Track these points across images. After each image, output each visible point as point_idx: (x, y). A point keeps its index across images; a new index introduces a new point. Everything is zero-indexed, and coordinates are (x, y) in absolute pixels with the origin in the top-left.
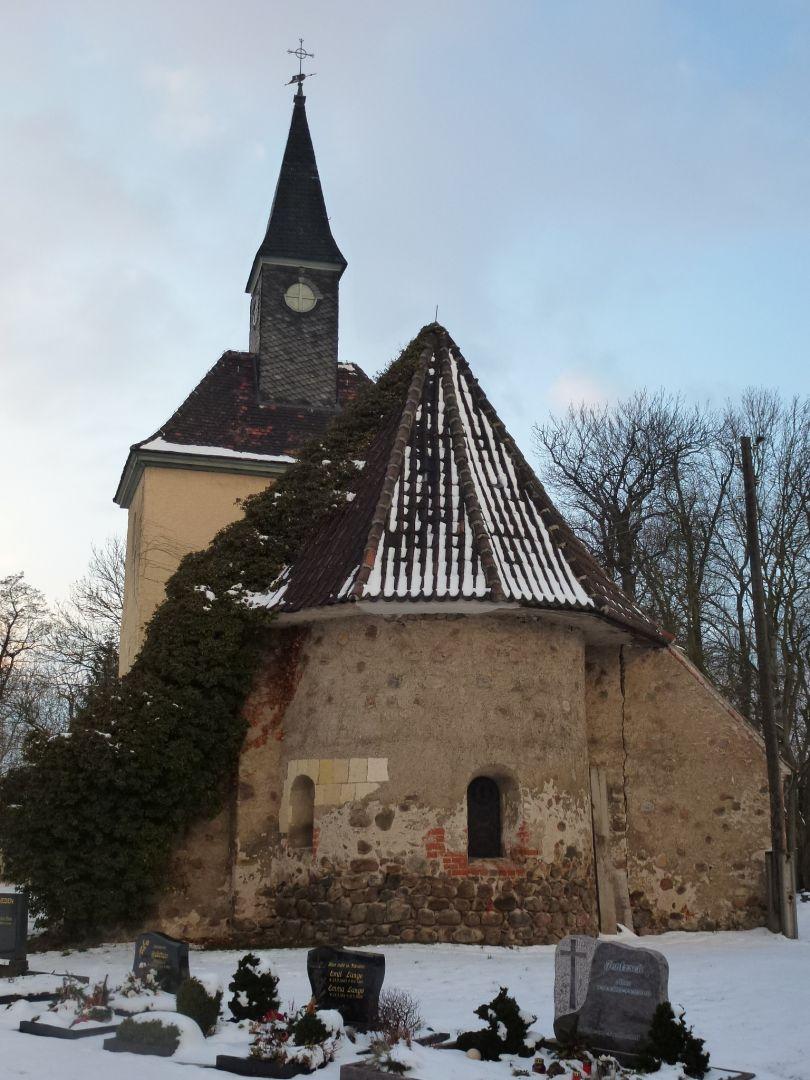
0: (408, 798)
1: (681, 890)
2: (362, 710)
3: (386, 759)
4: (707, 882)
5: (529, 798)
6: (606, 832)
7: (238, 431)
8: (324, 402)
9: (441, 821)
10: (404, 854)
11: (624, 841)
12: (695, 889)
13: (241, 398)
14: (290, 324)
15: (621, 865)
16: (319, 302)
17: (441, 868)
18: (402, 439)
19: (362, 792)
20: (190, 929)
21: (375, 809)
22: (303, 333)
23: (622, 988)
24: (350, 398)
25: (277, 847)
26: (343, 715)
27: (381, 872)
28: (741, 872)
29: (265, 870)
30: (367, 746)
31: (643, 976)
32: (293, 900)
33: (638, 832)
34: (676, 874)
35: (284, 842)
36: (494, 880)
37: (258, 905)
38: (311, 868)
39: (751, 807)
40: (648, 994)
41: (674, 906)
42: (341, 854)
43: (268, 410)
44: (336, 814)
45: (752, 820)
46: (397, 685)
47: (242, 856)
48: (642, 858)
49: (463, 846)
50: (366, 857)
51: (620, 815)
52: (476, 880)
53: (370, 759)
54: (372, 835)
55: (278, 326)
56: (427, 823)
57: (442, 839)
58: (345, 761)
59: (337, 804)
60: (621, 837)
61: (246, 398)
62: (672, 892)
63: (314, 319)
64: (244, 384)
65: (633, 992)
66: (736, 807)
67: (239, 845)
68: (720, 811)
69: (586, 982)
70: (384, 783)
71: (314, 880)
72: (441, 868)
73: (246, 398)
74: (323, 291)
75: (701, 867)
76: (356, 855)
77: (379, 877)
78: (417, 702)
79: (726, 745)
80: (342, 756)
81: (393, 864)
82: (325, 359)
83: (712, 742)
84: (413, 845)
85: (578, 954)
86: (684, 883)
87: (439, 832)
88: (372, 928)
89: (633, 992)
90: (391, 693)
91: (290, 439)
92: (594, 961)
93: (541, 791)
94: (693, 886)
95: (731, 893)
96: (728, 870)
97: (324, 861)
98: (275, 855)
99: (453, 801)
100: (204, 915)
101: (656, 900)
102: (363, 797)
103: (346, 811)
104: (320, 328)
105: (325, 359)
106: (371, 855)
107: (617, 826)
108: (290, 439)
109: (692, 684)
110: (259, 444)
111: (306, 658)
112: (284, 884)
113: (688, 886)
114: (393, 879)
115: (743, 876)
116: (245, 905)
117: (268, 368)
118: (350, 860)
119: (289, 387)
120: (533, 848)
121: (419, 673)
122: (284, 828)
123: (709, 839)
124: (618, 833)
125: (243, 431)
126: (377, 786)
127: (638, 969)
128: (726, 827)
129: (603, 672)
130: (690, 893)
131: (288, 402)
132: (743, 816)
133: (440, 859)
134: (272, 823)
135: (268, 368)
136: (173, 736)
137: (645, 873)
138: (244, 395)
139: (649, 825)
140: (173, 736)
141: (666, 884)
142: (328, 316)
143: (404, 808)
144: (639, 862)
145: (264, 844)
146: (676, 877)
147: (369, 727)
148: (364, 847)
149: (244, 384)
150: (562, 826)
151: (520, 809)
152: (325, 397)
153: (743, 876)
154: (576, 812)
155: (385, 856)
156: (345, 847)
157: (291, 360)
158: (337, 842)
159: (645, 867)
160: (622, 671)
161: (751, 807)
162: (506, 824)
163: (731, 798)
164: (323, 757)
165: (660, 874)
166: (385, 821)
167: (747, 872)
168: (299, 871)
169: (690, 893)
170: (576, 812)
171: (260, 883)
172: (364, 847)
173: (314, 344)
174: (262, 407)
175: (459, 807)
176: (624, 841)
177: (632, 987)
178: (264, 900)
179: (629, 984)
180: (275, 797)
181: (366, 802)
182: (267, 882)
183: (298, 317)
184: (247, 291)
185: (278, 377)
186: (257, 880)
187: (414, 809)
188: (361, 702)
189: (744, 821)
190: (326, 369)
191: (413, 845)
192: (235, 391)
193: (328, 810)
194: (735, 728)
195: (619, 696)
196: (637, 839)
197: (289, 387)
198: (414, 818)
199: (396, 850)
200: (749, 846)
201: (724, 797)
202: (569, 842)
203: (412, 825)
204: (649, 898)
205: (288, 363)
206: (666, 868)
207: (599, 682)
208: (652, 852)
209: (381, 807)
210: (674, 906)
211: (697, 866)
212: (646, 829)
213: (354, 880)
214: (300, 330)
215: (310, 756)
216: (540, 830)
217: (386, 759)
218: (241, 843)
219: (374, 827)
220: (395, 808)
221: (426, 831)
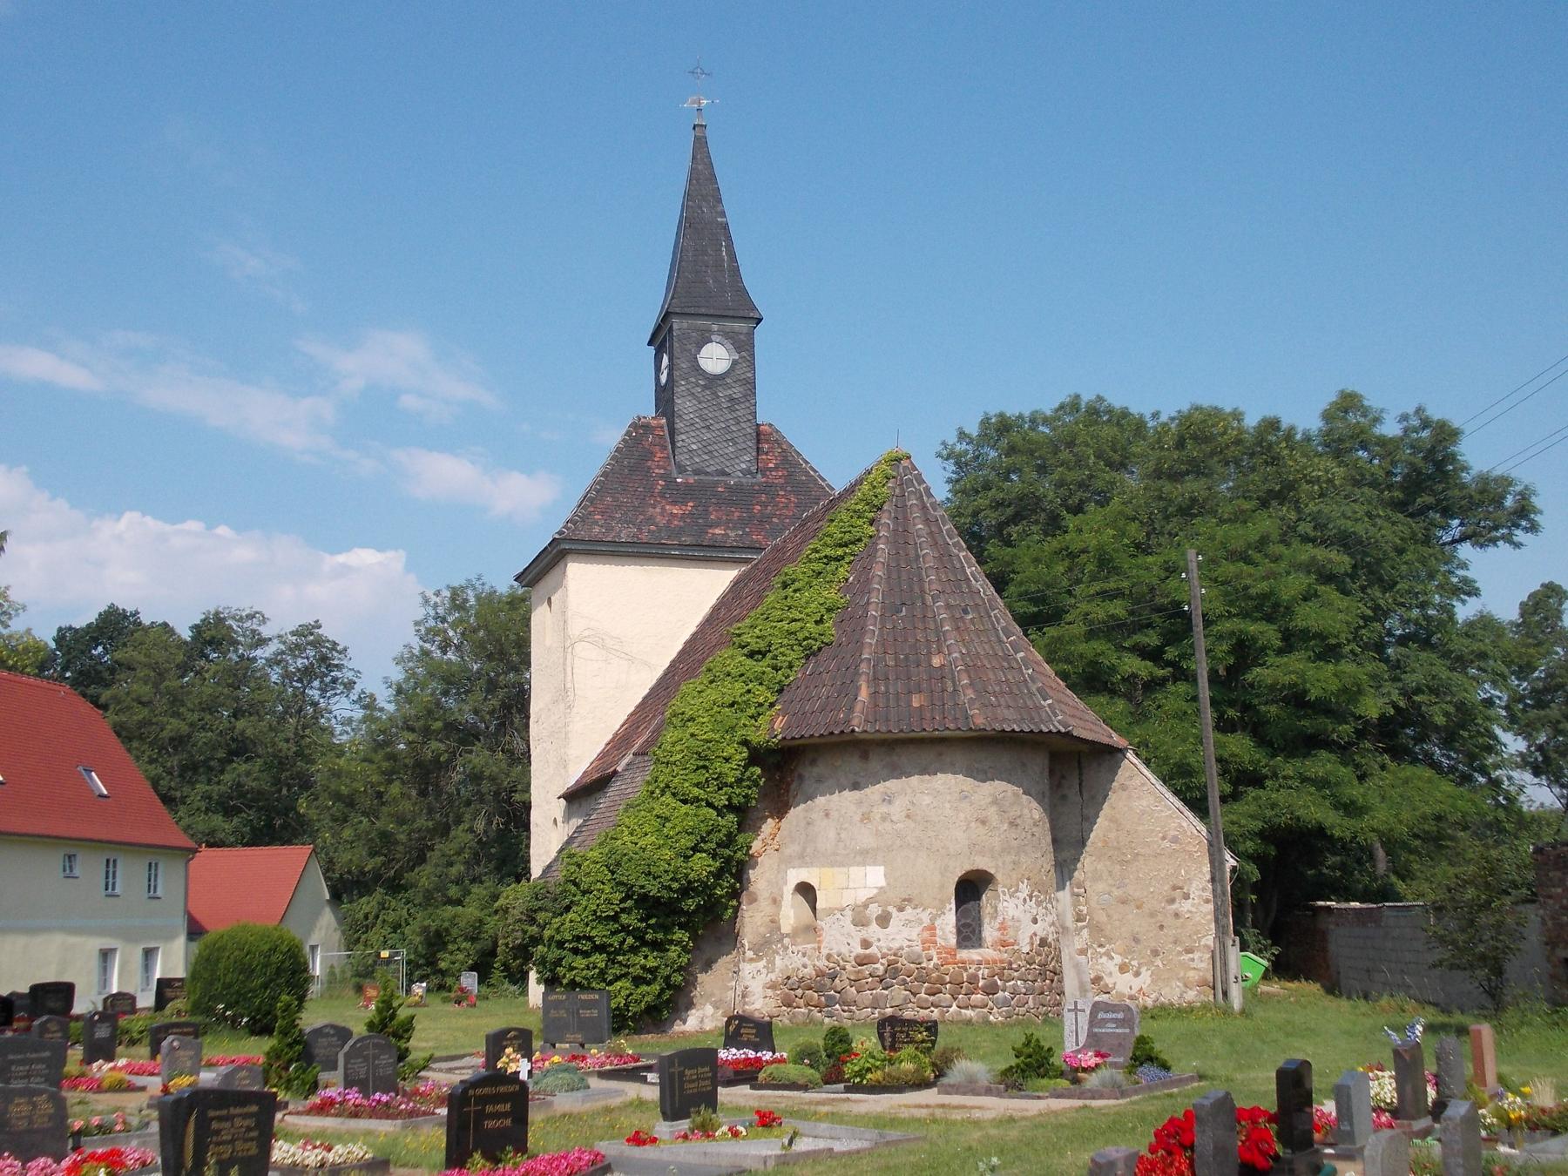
0: (904, 900)
1: (1137, 974)
2: (859, 824)
3: (882, 868)
4: (1161, 965)
5: (1007, 897)
6: (1069, 921)
7: (658, 510)
8: (746, 472)
9: (933, 919)
10: (901, 948)
11: (1085, 932)
12: (1150, 972)
13: (657, 471)
14: (705, 387)
15: (1083, 952)
16: (735, 363)
17: (935, 960)
18: (880, 573)
19: (863, 896)
20: (706, 1021)
21: (874, 910)
22: (718, 397)
23: (1110, 1028)
24: (771, 465)
25: (779, 946)
26: (841, 828)
27: (882, 964)
28: (1191, 956)
29: (770, 967)
30: (865, 856)
31: (1124, 1019)
32: (799, 992)
33: (1098, 922)
34: (1133, 959)
35: (786, 941)
36: (980, 969)
37: (766, 997)
38: (817, 963)
39: (1200, 896)
40: (1127, 1031)
41: (1131, 988)
42: (844, 950)
43: (686, 484)
44: (839, 915)
45: (1202, 909)
46: (890, 802)
47: (750, 954)
48: (1101, 946)
49: (953, 940)
50: (867, 951)
51: (1081, 908)
52: (966, 970)
53: (868, 867)
54: (874, 931)
55: (693, 391)
56: (920, 921)
57: (934, 935)
58: (845, 870)
59: (838, 906)
60: (1083, 927)
61: (662, 471)
62: (1129, 976)
63: (729, 381)
64: (658, 455)
65: (1117, 1031)
66: (1186, 896)
67: (747, 944)
68: (1172, 901)
69: (1086, 1027)
70: (881, 888)
71: (820, 974)
72: (935, 960)
73: (662, 471)
74: (738, 349)
75: (1155, 953)
76: (859, 950)
77: (880, 968)
78: (908, 816)
79: (1175, 840)
80: (842, 865)
81: (893, 958)
82: (743, 425)
83: (1164, 838)
84: (910, 941)
85: (1080, 1011)
86: (1139, 968)
87: (932, 928)
88: (876, 1011)
89: (1117, 1031)
90: (884, 809)
91: (712, 517)
92: (1091, 1013)
93: (1017, 891)
94: (1148, 969)
95: (1182, 974)
96: (1180, 953)
97: (829, 957)
98: (778, 953)
99: (943, 903)
100: (716, 1008)
101: (1115, 984)
102: (864, 900)
103: (848, 913)
104: (737, 392)
105: (743, 425)
106: (873, 950)
107: (1079, 918)
108: (712, 517)
109: (1143, 785)
110: (682, 524)
111: (801, 777)
112: (788, 978)
113: (1143, 969)
114: (893, 970)
115: (1193, 960)
116: (753, 998)
117: (684, 437)
118: (853, 955)
119: (707, 458)
120: (1012, 940)
121: (909, 791)
122: (786, 929)
123: (1161, 927)
124: (1080, 924)
125: (663, 508)
126: (875, 891)
127: (1120, 1016)
128: (1177, 915)
129: (1063, 777)
130: (1146, 975)
131: (707, 474)
132: (1193, 905)
133: (933, 952)
134: (774, 923)
135: (684, 437)
136: (695, 849)
137: (1104, 959)
138: (659, 467)
139: (1108, 916)
140: (695, 849)
141: (1123, 969)
142: (743, 376)
143: (901, 909)
144: (1099, 950)
145: (764, 947)
146: (1132, 963)
147: (865, 838)
148: (866, 944)
149: (658, 455)
150: (1035, 921)
151: (1000, 907)
152: (744, 466)
153: (1193, 960)
154: (1046, 908)
155: (885, 951)
156: (849, 944)
157: (708, 427)
158: (840, 940)
159: (1105, 954)
160: (1081, 774)
161: (1200, 896)
162: (986, 921)
163: (1181, 888)
164: (823, 866)
165: (1118, 959)
166: (884, 920)
167: (1196, 955)
168: (805, 966)
169: (1146, 975)
170: (1046, 908)
171: (764, 978)
172: (866, 944)
173: (731, 409)
174: (679, 480)
175: (948, 907)
176: (1085, 932)
177: (1117, 1028)
178: (770, 992)
179: (1114, 1026)
180: (776, 902)
181: (866, 906)
182: (773, 976)
183: (714, 381)
184: (650, 344)
185: (694, 447)
186: (763, 976)
187: (909, 910)
188: (857, 818)
189: (1194, 910)
190: (744, 435)
191: (910, 941)
192: (649, 463)
193: (830, 912)
194: (1185, 824)
195: (1078, 798)
196: (1096, 929)
197: (707, 458)
198: (909, 918)
199: (895, 945)
200: (1198, 932)
201: (1175, 888)
202: (1041, 934)
203: (907, 923)
204: (1109, 981)
205: (704, 431)
206: (1123, 954)
207: (1059, 786)
208: (1110, 940)
209: (880, 909)
210: (1131, 988)
211: (1152, 951)
212: (1104, 919)
213: (859, 972)
214: (715, 393)
215: (811, 865)
216: (1017, 924)
217: (882, 868)
218: (749, 942)
219: (874, 926)
220: (891, 909)
221: (921, 928)
